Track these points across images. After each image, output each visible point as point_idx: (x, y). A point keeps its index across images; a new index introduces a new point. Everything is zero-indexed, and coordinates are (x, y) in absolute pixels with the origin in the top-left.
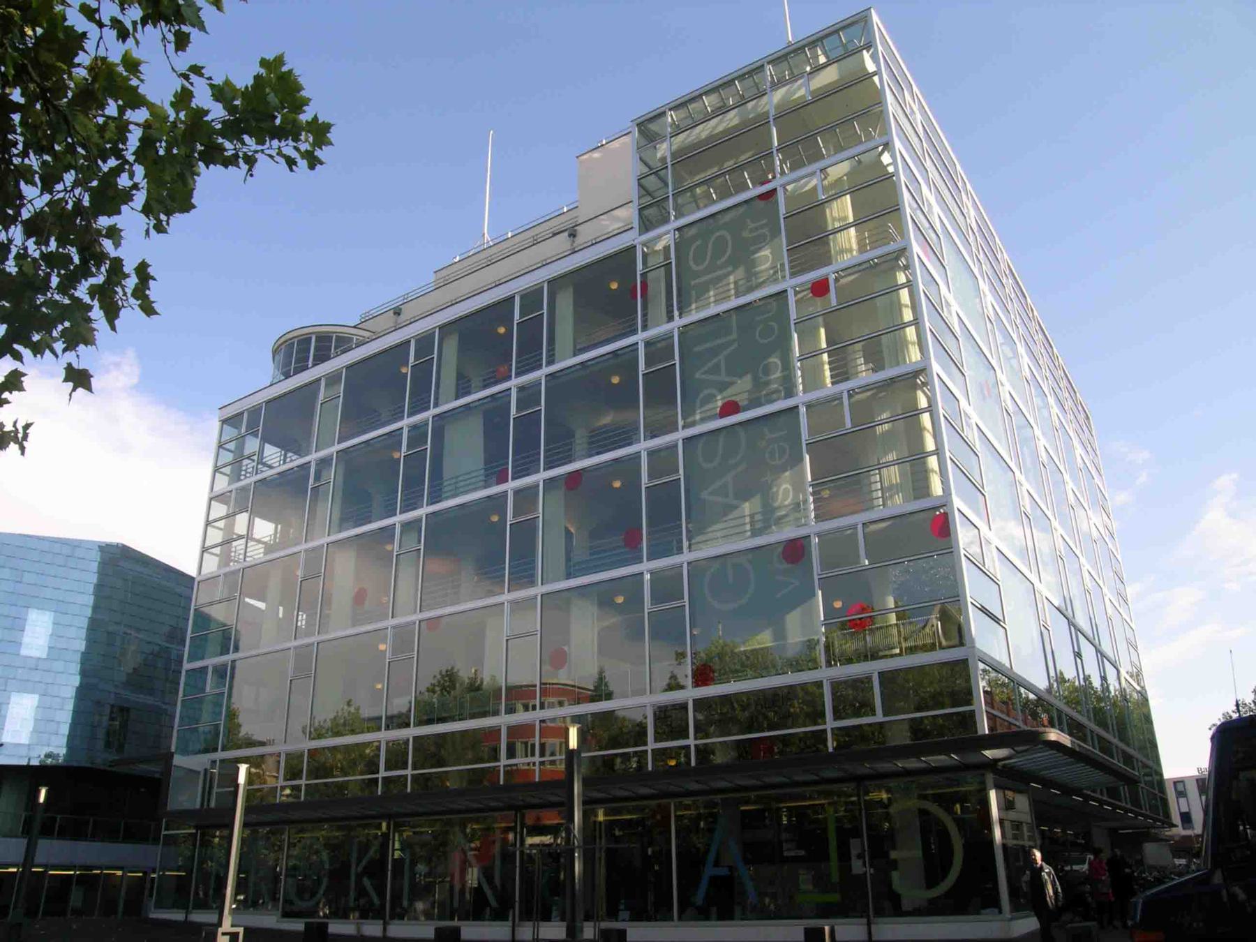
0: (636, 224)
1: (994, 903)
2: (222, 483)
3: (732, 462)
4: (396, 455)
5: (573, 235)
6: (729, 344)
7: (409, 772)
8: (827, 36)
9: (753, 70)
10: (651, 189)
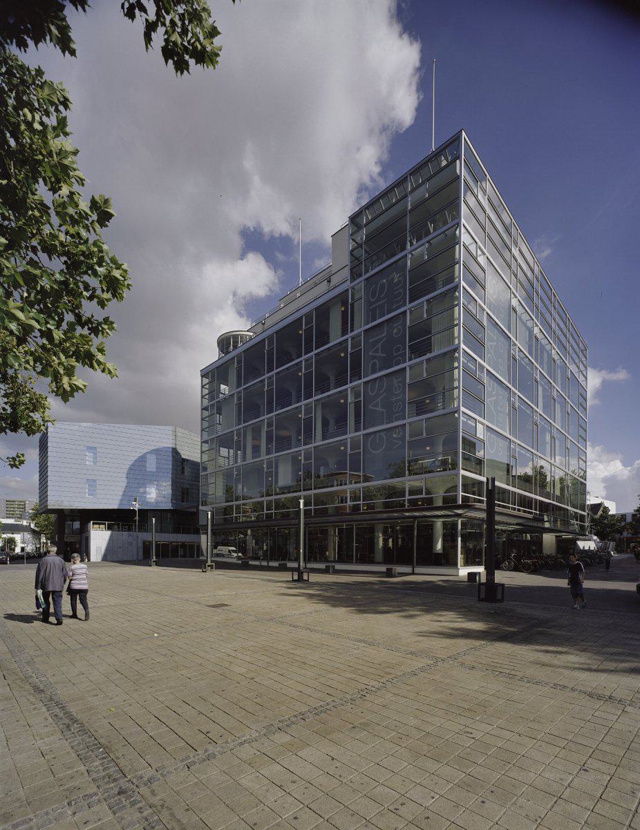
0: (349, 278)
1: (157, 546)
2: (206, 402)
3: (381, 392)
4: (300, 374)
5: (329, 281)
6: (381, 339)
7: (312, 507)
8: (446, 147)
9: (420, 167)
10: (357, 257)
